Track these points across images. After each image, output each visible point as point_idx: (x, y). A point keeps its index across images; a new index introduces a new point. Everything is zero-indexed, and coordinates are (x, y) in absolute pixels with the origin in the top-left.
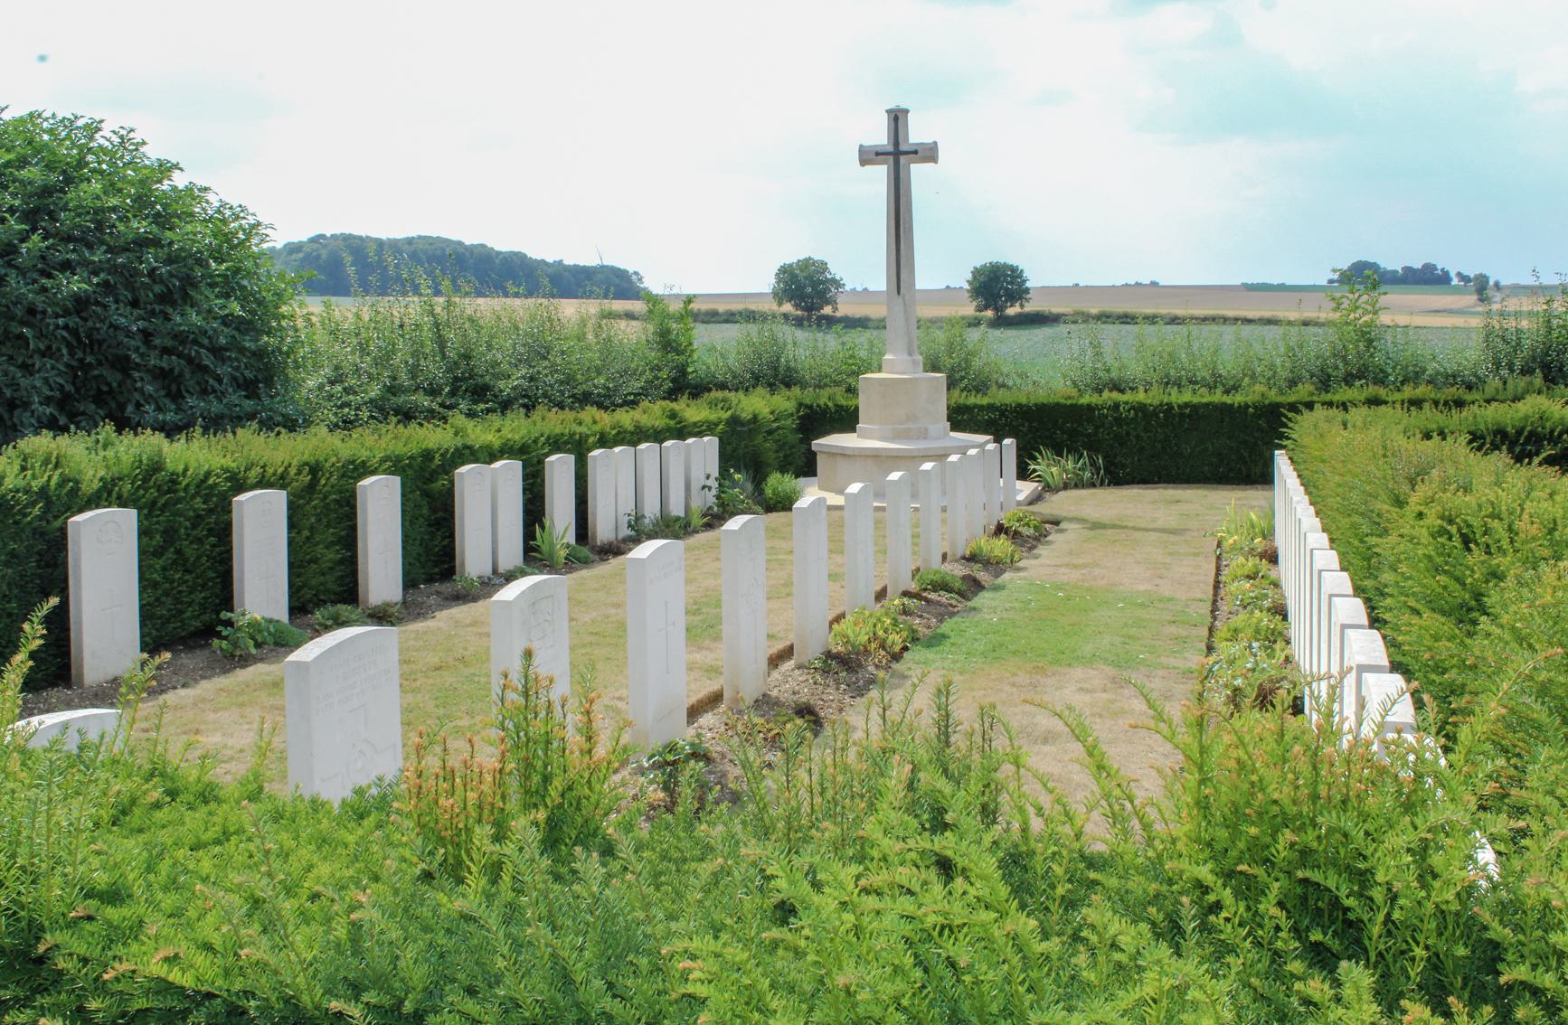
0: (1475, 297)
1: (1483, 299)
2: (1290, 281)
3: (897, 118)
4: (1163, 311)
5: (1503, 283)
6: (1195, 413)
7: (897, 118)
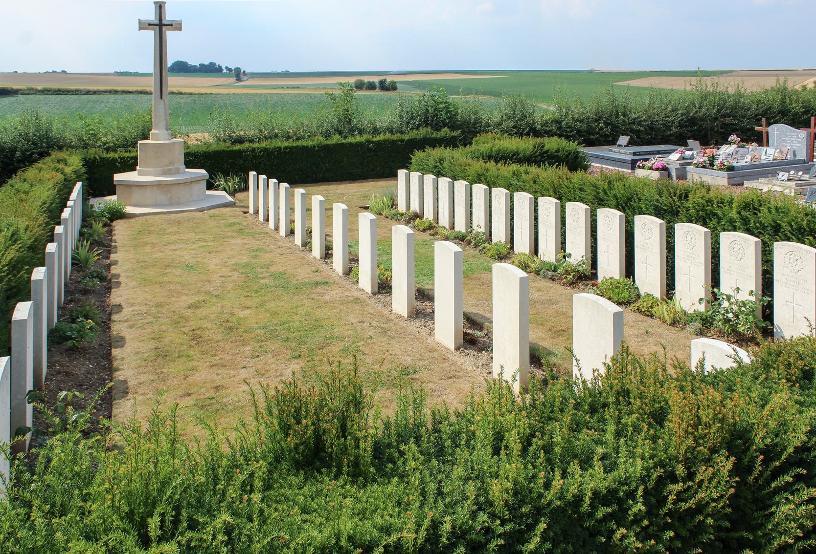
1: (239, 79)
3: (160, 7)
4: (81, 88)
5: (247, 72)
6: (292, 151)
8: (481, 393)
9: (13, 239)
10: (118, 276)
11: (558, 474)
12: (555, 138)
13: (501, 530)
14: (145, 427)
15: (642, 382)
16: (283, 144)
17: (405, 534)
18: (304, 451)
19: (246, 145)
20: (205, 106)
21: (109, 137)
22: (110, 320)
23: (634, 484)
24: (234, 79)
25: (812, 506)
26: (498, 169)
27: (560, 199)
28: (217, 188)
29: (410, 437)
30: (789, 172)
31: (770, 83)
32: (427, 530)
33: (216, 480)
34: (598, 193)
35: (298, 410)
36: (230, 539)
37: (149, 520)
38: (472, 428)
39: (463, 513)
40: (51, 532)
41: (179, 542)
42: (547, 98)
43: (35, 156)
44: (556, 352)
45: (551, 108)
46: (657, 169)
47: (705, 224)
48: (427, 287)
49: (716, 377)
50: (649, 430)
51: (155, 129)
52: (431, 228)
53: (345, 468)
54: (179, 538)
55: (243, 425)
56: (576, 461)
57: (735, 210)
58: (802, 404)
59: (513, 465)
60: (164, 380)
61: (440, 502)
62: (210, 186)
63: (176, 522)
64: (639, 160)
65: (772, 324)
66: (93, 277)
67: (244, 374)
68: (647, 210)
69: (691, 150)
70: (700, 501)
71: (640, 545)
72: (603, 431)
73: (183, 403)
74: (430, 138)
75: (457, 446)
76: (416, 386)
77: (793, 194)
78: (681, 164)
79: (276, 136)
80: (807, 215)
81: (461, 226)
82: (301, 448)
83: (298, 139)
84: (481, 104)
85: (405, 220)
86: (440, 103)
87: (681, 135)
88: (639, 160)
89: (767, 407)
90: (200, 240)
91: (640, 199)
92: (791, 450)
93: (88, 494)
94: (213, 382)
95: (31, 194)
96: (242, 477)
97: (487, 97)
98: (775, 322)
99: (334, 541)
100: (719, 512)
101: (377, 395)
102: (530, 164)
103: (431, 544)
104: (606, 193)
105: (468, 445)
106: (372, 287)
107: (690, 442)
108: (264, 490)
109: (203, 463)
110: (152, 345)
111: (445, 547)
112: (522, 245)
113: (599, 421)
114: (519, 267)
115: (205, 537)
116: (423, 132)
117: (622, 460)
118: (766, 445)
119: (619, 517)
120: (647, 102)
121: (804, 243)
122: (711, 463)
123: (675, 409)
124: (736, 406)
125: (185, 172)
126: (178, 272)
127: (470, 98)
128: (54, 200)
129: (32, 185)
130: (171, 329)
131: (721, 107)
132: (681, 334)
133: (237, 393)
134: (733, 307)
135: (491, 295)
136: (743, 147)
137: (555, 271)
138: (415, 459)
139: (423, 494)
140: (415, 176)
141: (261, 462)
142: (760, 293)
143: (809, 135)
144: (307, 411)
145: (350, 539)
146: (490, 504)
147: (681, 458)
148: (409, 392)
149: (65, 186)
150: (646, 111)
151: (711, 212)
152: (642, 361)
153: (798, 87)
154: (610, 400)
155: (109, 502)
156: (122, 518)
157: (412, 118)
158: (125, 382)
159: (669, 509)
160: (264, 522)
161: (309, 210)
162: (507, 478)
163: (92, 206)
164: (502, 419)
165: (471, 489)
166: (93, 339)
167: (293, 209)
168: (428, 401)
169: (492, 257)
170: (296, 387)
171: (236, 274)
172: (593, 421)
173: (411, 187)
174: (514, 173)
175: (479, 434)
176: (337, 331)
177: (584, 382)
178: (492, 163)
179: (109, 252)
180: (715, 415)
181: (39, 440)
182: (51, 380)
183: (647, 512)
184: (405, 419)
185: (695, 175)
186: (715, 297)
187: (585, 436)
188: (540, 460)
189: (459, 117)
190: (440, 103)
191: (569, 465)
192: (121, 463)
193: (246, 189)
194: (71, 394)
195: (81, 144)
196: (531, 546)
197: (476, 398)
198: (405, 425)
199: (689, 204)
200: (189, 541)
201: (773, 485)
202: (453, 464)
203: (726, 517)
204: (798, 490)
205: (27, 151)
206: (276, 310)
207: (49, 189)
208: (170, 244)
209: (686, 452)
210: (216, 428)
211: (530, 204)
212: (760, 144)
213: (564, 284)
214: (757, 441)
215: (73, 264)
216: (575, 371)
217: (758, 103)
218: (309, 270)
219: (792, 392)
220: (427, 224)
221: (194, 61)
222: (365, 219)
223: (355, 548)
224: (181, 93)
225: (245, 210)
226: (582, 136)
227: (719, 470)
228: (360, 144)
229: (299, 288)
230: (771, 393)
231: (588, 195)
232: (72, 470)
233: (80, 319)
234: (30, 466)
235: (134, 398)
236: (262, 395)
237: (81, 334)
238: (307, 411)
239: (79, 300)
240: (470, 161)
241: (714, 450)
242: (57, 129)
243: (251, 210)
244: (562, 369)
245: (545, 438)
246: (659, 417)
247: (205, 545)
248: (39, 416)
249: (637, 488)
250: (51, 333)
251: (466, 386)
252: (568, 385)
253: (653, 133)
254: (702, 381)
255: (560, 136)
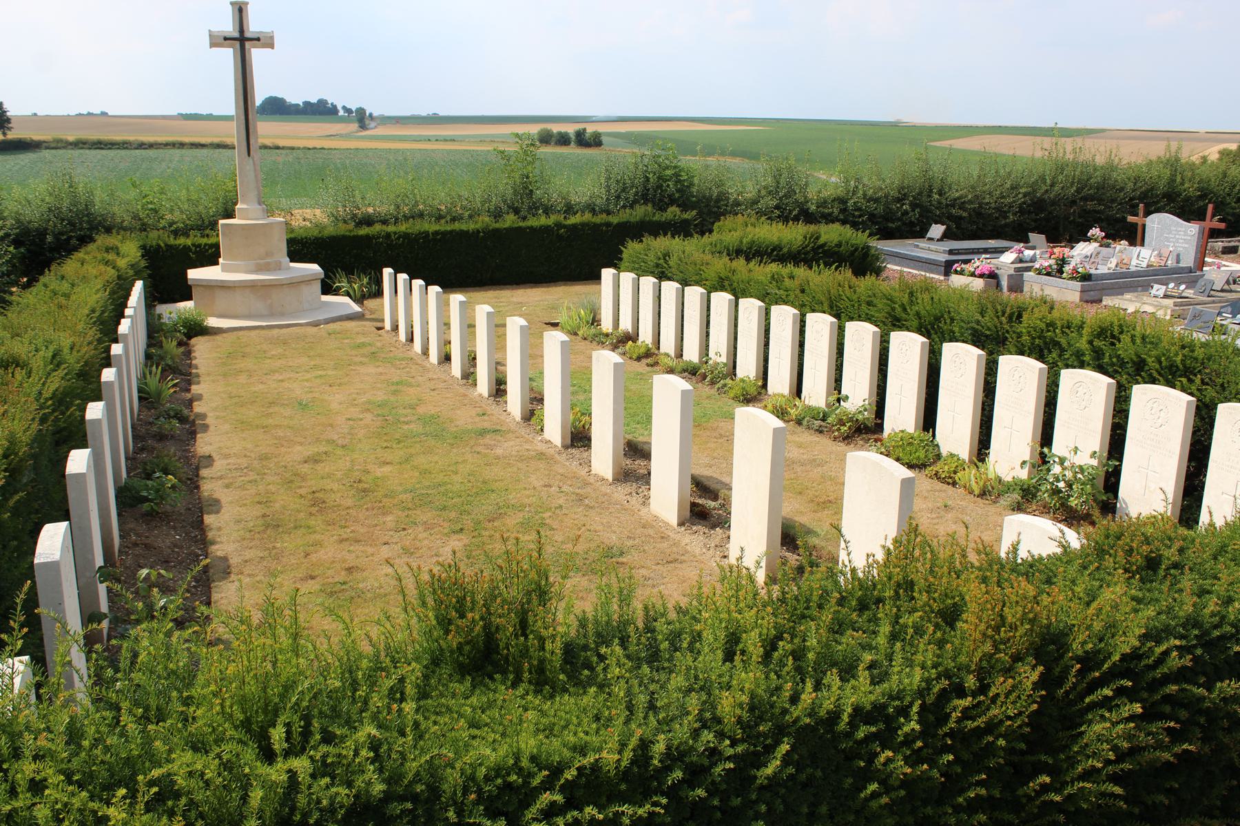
0: (357, 125)
1: (363, 127)
2: (216, 112)
3: (240, 12)
4: (131, 138)
5: (375, 114)
7: (240, 12)
8: (711, 583)
9: (55, 362)
10: (204, 416)
11: (809, 685)
12: (837, 226)
13: (730, 752)
14: (256, 618)
15: (931, 571)
16: (432, 227)
17: (604, 754)
18: (470, 652)
19: (378, 228)
20: (309, 169)
21: (177, 213)
22: (197, 476)
23: (909, 699)
24: (355, 126)
25: (1132, 725)
26: (750, 271)
27: (837, 316)
28: (336, 292)
29: (614, 637)
30: (1167, 284)
31: (1156, 150)
32: (633, 750)
33: (355, 685)
34: (893, 309)
35: (461, 601)
36: (377, 756)
37: (271, 730)
38: (698, 627)
39: (681, 731)
40: (148, 741)
41: (311, 757)
42: (828, 164)
43: (74, 242)
44: (818, 530)
45: (833, 179)
46: (981, 276)
47: (1041, 358)
48: (641, 439)
49: (1031, 566)
50: (935, 632)
51: (243, 202)
52: (650, 356)
53: (526, 675)
54: (312, 753)
55: (388, 618)
56: (834, 671)
57: (1085, 339)
58: (1138, 601)
59: (751, 674)
60: (277, 558)
61: (651, 718)
62: (327, 289)
63: (306, 733)
64: (957, 261)
65: (1116, 497)
66: (170, 417)
67: (385, 552)
68: (962, 335)
69: (1033, 248)
70: (991, 719)
71: (909, 770)
72: (874, 633)
73: (305, 588)
74: (650, 222)
75: (676, 650)
76: (623, 573)
77: (1168, 317)
78: (1017, 270)
79: (421, 215)
80: (1183, 347)
81: (692, 354)
82: (467, 648)
83: (454, 219)
84: (728, 170)
85: (611, 344)
86: (667, 168)
87: (1020, 225)
88: (957, 261)
89: (1094, 605)
90: (315, 367)
91: (952, 320)
92: (1116, 657)
93: (190, 697)
94: (345, 561)
95: (73, 297)
96: (389, 683)
97: (737, 160)
98: (1120, 495)
99: (512, 762)
100: (1014, 731)
101: (569, 583)
102: (796, 264)
103: (639, 767)
104: (905, 310)
105: (691, 648)
106: (563, 438)
107: (988, 647)
108: (419, 699)
109: (337, 664)
110: (258, 511)
111: (657, 770)
112: (779, 382)
113: (869, 621)
114: (773, 413)
115: (344, 752)
116: (641, 212)
117: (896, 669)
118: (1086, 652)
119: (886, 738)
120: (975, 174)
121: (1174, 387)
122: (1012, 674)
123: (973, 607)
124: (1053, 603)
125: (289, 268)
126: (287, 412)
127: (712, 160)
128: (106, 307)
129: (73, 285)
130: (282, 491)
131: (1083, 184)
132: (992, 509)
133: (378, 577)
134: (1067, 473)
135: (731, 452)
136: (1108, 246)
137: (824, 420)
138: (619, 665)
139: (630, 708)
140: (627, 278)
141: (414, 664)
142: (1105, 454)
143: (1202, 232)
144: (473, 602)
145: (533, 759)
146: (718, 720)
147: (973, 667)
148: (614, 580)
149: (120, 287)
150: (973, 187)
151: (1052, 340)
152: (935, 543)
153: (1195, 159)
154: (887, 594)
155: (218, 708)
156: (236, 728)
157: (623, 190)
158: (225, 559)
159: (951, 729)
160: (421, 737)
161: (472, 326)
162: (742, 690)
163: (160, 316)
164: (739, 617)
165: (693, 703)
166: (178, 501)
167: (448, 325)
168: (639, 592)
169: (735, 398)
170: (458, 570)
171: (369, 416)
172: (861, 621)
173: (620, 293)
174: (773, 277)
175: (708, 635)
176: (512, 498)
177: (853, 570)
178: (742, 261)
179: (190, 383)
180: (1025, 614)
181: (119, 630)
182: (127, 554)
183: (922, 732)
184: (607, 615)
185: (1035, 286)
186: (1044, 460)
187: (849, 639)
188: (786, 669)
189: (694, 190)
190: (667, 168)
191: (825, 674)
192: (229, 662)
193: (379, 293)
194: (154, 573)
195: (138, 225)
196: (769, 770)
197: (704, 589)
198: (607, 623)
199: (1022, 328)
200: (325, 756)
201: (1087, 700)
202: (671, 672)
203: (1023, 737)
204: (1118, 706)
205: (62, 233)
206: (427, 467)
207: (98, 290)
208: (274, 372)
209: (981, 660)
210: (352, 621)
211: (794, 323)
212: (1132, 243)
213: (835, 438)
214: (1074, 646)
215: (140, 398)
216: (843, 556)
217: (1137, 179)
218: (473, 413)
219: (1129, 585)
220: (643, 350)
221: (295, 97)
222: (554, 340)
223: (540, 770)
224: (278, 148)
225: (379, 325)
226: (876, 223)
227: (1020, 682)
228: (546, 229)
229: (459, 438)
230: (1101, 586)
231: (879, 311)
232: (166, 668)
233: (157, 475)
234: (112, 661)
235: (240, 580)
236: (412, 580)
237: (160, 494)
238: (473, 602)
239: (154, 448)
240: (708, 257)
241: (1017, 658)
242: (101, 202)
243: (388, 326)
244: (824, 553)
245: (796, 641)
246: (950, 616)
247: (345, 762)
248: (116, 599)
249: (911, 704)
250: (121, 492)
251: (691, 574)
252: (832, 574)
253: (986, 217)
254: (1013, 570)
255: (844, 222)
